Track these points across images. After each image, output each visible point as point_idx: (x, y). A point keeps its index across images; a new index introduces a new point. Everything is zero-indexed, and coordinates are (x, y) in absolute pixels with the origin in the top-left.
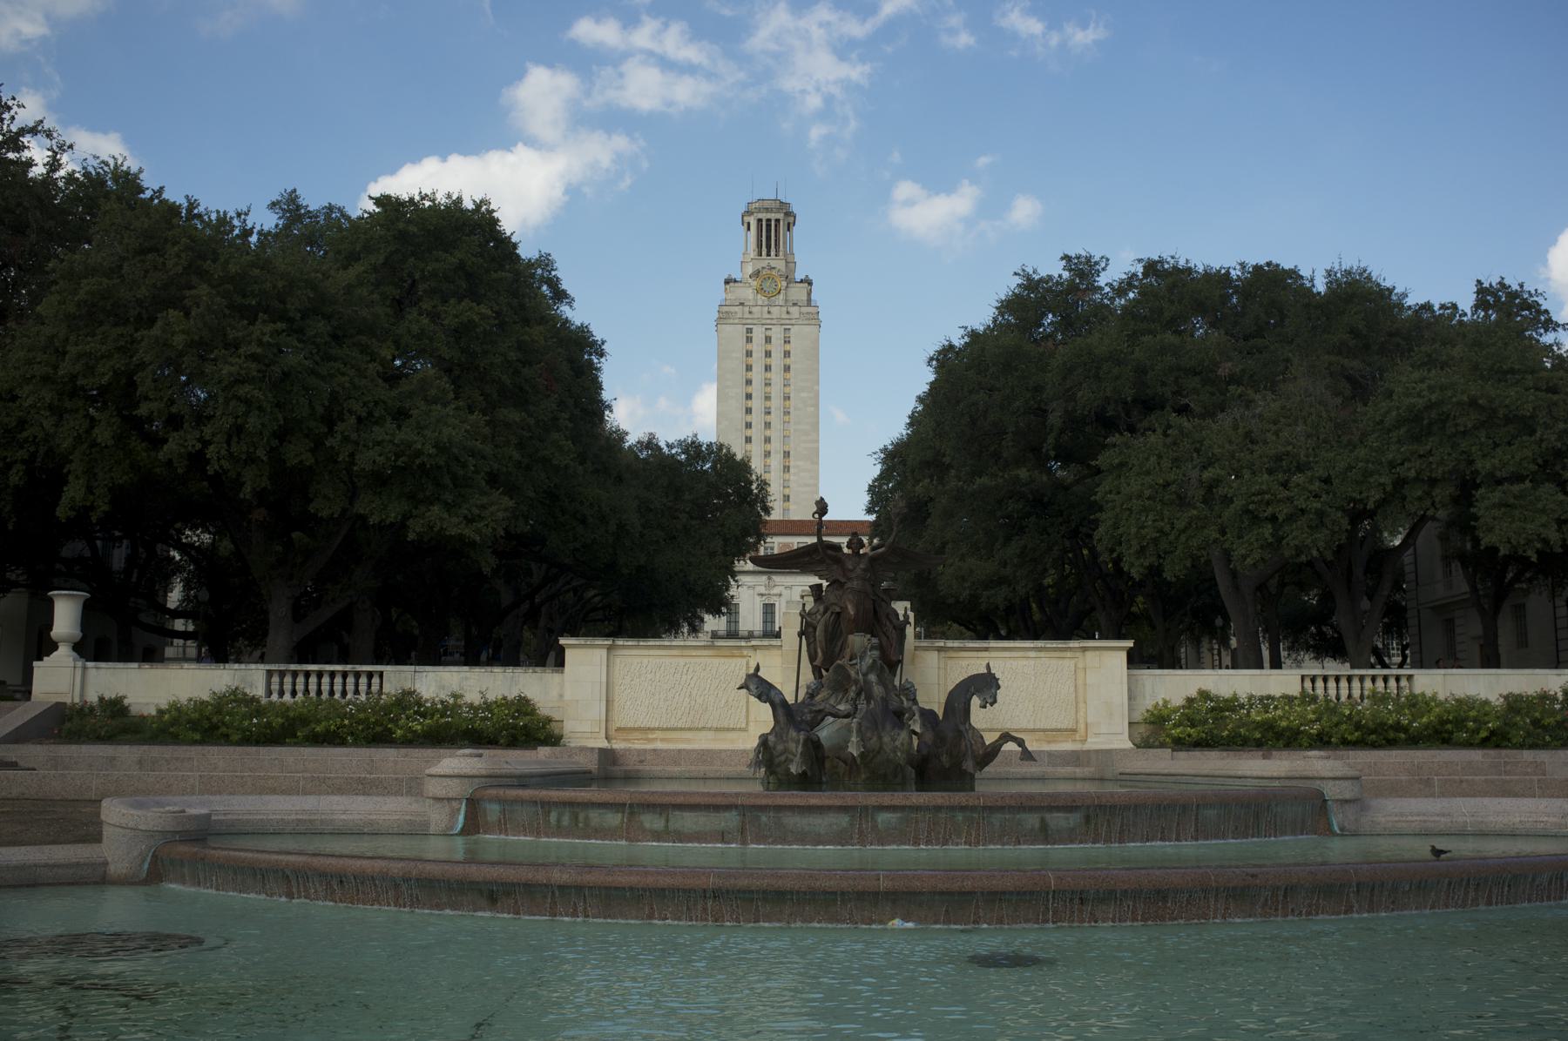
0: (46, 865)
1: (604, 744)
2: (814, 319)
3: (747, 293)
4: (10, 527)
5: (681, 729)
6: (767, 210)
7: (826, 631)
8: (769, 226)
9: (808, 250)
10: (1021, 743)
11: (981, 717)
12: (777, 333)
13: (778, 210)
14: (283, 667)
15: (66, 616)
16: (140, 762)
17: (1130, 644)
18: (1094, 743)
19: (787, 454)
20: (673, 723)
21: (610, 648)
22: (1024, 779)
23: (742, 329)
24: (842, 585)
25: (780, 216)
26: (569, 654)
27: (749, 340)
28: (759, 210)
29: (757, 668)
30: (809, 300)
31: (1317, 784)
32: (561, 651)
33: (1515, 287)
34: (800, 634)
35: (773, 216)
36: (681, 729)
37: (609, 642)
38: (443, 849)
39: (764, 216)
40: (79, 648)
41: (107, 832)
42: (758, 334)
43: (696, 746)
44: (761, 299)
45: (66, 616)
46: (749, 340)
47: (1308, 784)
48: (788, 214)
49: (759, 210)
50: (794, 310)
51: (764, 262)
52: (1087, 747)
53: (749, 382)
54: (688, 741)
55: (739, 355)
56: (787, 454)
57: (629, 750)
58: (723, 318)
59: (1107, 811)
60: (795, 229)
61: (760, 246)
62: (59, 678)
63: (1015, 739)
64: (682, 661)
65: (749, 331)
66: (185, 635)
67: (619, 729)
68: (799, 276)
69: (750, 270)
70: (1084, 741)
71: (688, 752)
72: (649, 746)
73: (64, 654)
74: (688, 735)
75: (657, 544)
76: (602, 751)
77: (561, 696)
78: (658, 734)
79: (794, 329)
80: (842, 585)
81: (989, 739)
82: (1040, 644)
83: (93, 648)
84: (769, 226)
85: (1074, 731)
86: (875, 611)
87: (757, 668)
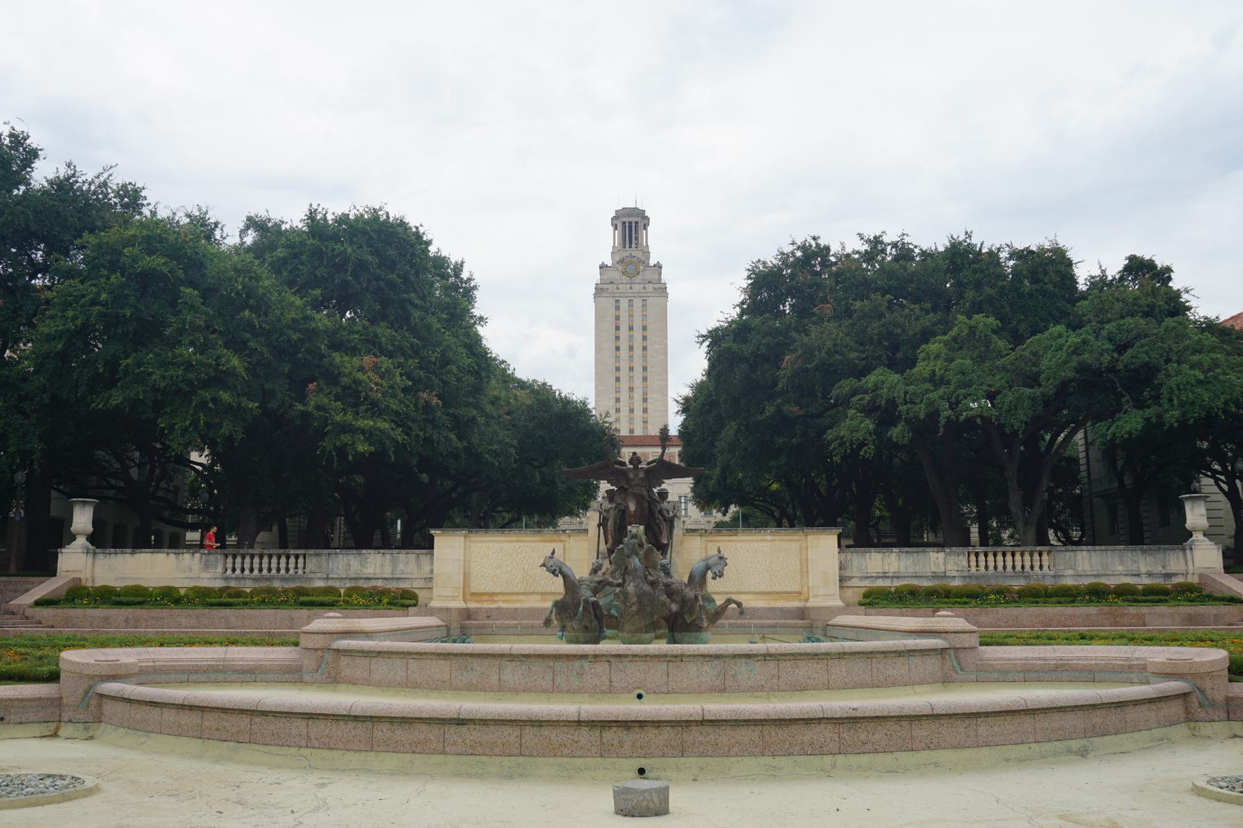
0: (18, 699)
1: (462, 605)
2: (662, 291)
3: (615, 275)
4: (100, 453)
5: (517, 594)
6: (629, 215)
7: (615, 522)
8: (630, 227)
10: (739, 605)
11: (712, 585)
12: (638, 303)
13: (637, 215)
14: (271, 552)
15: (82, 519)
16: (126, 621)
18: (813, 603)
20: (511, 590)
23: (612, 301)
24: (626, 490)
25: (638, 219)
26: (436, 540)
27: (617, 308)
29: (553, 553)
32: (432, 538)
33: (738, 310)
34: (599, 526)
35: (633, 220)
36: (517, 594)
39: (627, 220)
40: (92, 539)
41: (63, 675)
42: (624, 303)
43: (526, 605)
45: (82, 519)
46: (617, 308)
50: (650, 287)
52: (809, 604)
53: (617, 338)
54: (521, 601)
55: (611, 319)
57: (480, 609)
58: (599, 291)
62: (76, 562)
63: (734, 602)
64: (517, 545)
65: (617, 301)
67: (473, 594)
70: (807, 600)
71: (522, 609)
72: (494, 606)
73: (81, 541)
74: (522, 597)
75: (533, 460)
76: (460, 611)
77: (432, 571)
78: (501, 598)
79: (650, 300)
80: (626, 490)
81: (719, 601)
83: (101, 539)
84: (630, 227)
85: (800, 593)
86: (650, 509)
87: (553, 553)
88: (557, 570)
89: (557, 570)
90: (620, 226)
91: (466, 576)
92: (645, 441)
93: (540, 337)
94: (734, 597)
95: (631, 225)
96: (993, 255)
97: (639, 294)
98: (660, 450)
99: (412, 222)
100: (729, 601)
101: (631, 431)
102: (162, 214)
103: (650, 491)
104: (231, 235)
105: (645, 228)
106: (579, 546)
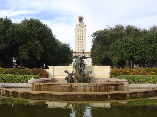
2: (86, 29)
3: (78, 27)
6: (81, 17)
9: (85, 21)
10: (94, 77)
12: (82, 31)
17: (110, 66)
19: (83, 45)
21: (53, 67)
22: (135, 88)
26: (49, 67)
28: (80, 17)
30: (85, 28)
31: (123, 82)
32: (48, 67)
35: (81, 18)
37: (53, 66)
38: (29, 91)
42: (80, 31)
44: (80, 27)
47: (122, 82)
48: (83, 18)
49: (80, 17)
50: (84, 28)
51: (80, 23)
56: (83, 45)
58: (76, 30)
59: (106, 87)
60: (84, 19)
61: (80, 21)
66: (16, 65)
68: (84, 25)
69: (79, 24)
74: (62, 76)
75: (62, 55)
82: (105, 66)
88: (67, 72)
89: (67, 72)
90: (79, 19)
91: (58, 81)
92: (80, 53)
93: (63, 34)
94: (93, 76)
95: (81, 19)
96: (151, 30)
97: (82, 30)
98: (83, 54)
99: (124, 24)
100: (92, 77)
101: (81, 51)
102: (115, 27)
103: (81, 60)
104: (59, 41)
105: (83, 19)
106: (71, 69)
